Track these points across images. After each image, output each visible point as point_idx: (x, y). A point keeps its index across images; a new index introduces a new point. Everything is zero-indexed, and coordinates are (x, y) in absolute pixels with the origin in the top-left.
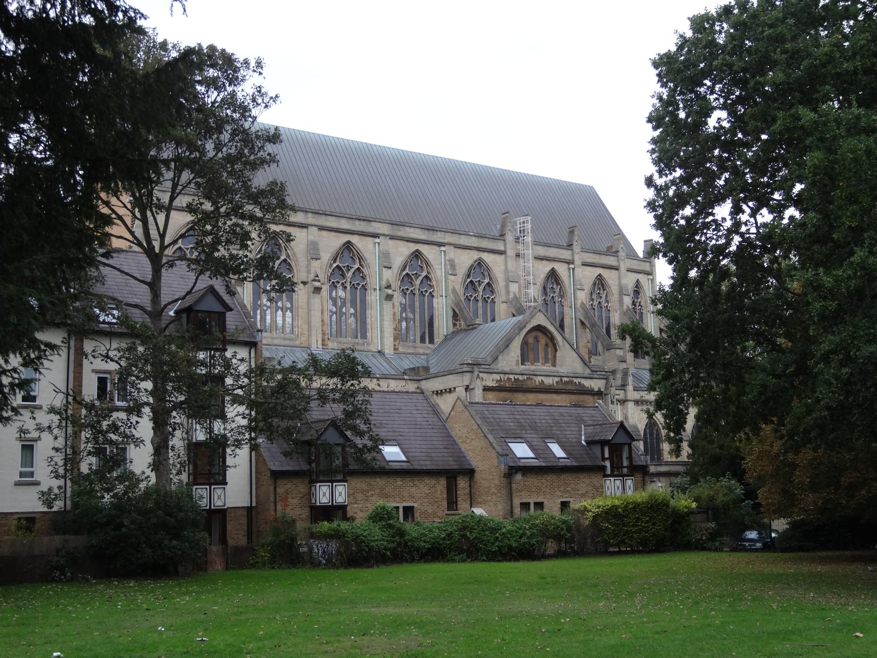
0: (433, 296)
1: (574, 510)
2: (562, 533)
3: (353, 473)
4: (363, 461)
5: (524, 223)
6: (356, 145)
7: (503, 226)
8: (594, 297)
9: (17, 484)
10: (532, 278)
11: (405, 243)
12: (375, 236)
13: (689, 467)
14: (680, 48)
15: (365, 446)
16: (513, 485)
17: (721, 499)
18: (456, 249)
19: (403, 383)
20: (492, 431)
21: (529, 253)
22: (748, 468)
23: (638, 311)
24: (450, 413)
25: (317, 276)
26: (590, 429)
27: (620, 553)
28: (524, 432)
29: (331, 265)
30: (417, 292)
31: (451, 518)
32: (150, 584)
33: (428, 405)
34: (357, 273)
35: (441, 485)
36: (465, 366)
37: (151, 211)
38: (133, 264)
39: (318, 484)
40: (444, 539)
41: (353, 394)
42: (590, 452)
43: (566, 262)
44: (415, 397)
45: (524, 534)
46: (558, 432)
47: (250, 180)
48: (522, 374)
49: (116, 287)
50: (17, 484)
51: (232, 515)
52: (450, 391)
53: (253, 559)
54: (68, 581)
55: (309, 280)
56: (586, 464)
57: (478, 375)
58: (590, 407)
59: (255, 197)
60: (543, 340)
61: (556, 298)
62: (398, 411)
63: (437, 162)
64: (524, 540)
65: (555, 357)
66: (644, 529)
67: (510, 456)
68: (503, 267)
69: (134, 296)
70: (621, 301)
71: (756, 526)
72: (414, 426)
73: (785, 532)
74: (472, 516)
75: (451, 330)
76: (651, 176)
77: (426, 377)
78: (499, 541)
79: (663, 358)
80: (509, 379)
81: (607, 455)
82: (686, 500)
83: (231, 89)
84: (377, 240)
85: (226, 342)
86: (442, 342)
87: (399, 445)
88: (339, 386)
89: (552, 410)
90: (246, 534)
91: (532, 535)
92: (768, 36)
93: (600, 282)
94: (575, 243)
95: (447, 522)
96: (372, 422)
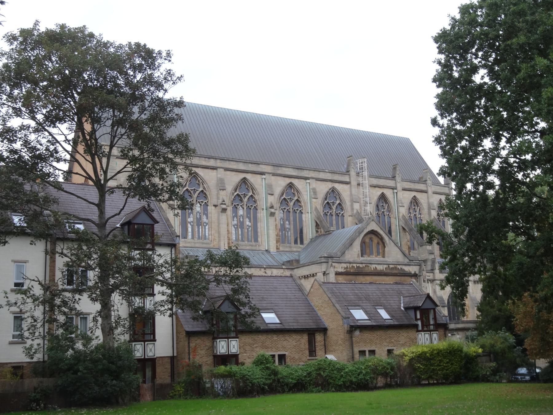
0: (302, 213)
1: (396, 355)
2: (388, 371)
3: (242, 332)
4: (244, 323)
5: (362, 163)
6: (250, 115)
7: (348, 165)
8: (411, 211)
9: (11, 343)
10: (368, 199)
11: (283, 178)
12: (262, 174)
13: (478, 324)
14: (453, 27)
15: (247, 313)
16: (354, 339)
17: (499, 346)
18: (317, 182)
19: (282, 271)
20: (339, 302)
21: (366, 182)
22: (517, 324)
23: (441, 220)
24: (310, 290)
25: (224, 201)
26: (407, 299)
27: (429, 385)
28: (361, 302)
29: (233, 194)
30: (291, 210)
31: (310, 362)
32: (97, 411)
33: (295, 285)
34: (251, 198)
35: (305, 338)
36: (323, 258)
37: (98, 156)
38: (93, 194)
39: (218, 340)
40: (305, 376)
41: (238, 278)
42: (407, 315)
43: (392, 189)
44: (287, 280)
45: (361, 372)
46: (385, 302)
47: (165, 133)
48: (362, 263)
49: (81, 209)
50: (11, 343)
51: (160, 362)
52: (313, 276)
53: (172, 393)
54: (42, 410)
55: (219, 204)
56: (404, 323)
57: (332, 265)
58: (406, 284)
59: (168, 144)
60: (375, 240)
61: (386, 213)
62: (274, 289)
63: (304, 124)
64: (361, 376)
65: (384, 251)
66: (446, 368)
67: (351, 318)
68: (349, 193)
69: (93, 215)
70: (429, 214)
71: (524, 364)
72: (285, 299)
73: (546, 368)
74: (325, 360)
75: (315, 234)
76: (436, 118)
77: (297, 266)
78: (344, 378)
79: (449, 247)
80: (353, 267)
81: (418, 317)
82: (474, 347)
83: (150, 72)
84: (264, 177)
85: (155, 244)
86: (309, 244)
87: (275, 312)
88: (228, 272)
89: (380, 287)
90: (170, 375)
91: (367, 373)
92: (513, 11)
93: (415, 202)
94: (397, 176)
95: (307, 365)
96: (251, 297)
